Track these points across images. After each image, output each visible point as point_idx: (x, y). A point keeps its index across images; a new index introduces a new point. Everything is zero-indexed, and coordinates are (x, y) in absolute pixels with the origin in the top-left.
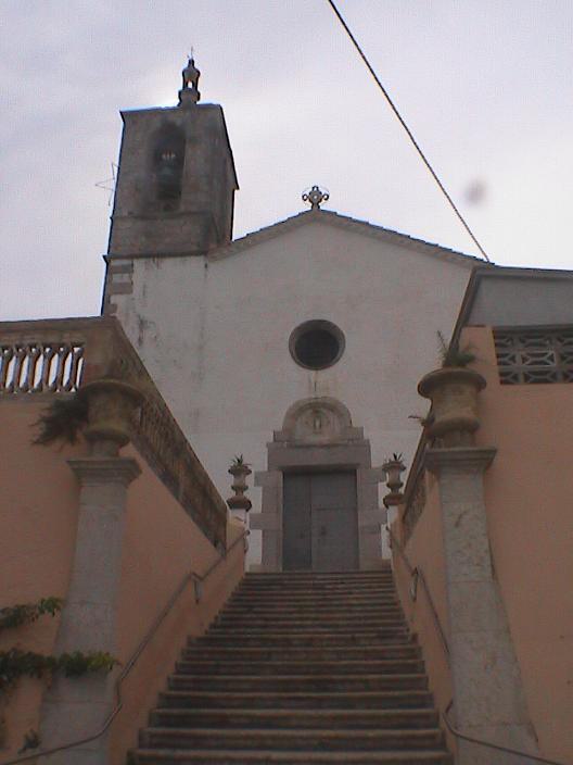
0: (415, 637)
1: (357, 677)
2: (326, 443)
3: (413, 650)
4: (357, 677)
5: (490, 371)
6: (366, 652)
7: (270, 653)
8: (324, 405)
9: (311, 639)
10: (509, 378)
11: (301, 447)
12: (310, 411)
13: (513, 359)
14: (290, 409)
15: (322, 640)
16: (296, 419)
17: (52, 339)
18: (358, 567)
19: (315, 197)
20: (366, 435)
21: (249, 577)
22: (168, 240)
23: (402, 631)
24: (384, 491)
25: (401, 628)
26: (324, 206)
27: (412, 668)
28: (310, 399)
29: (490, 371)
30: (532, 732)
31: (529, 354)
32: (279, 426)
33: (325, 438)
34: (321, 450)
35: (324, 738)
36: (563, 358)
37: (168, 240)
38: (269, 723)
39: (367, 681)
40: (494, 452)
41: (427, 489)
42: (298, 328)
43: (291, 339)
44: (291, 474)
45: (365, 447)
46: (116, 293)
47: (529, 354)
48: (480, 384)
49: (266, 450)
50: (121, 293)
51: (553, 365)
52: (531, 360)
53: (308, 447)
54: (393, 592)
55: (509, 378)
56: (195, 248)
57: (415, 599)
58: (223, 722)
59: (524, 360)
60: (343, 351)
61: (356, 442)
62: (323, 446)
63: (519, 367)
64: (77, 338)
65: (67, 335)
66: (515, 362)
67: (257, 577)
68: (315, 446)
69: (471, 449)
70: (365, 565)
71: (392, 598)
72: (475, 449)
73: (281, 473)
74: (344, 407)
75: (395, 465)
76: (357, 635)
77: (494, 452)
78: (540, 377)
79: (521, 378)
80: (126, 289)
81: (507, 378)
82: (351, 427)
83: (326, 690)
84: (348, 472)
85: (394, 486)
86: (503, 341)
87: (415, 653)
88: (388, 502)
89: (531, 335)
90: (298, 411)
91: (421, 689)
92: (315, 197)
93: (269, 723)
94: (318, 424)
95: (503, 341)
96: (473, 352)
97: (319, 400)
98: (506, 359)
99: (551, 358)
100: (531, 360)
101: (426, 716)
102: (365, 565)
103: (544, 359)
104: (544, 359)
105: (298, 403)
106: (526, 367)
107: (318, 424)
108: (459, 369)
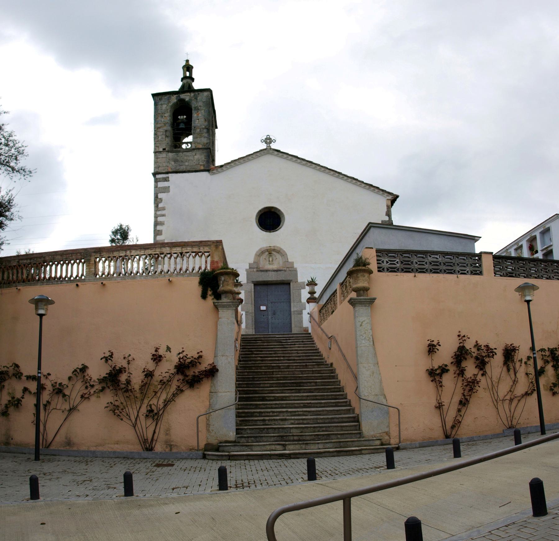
0: (332, 364)
1: (312, 381)
2: (276, 269)
3: (332, 370)
4: (312, 381)
5: (373, 266)
6: (313, 371)
7: (273, 372)
8: (274, 250)
9: (289, 366)
10: (381, 269)
11: (261, 271)
12: (267, 253)
13: (383, 262)
14: (257, 252)
15: (293, 366)
16: (260, 257)
17: (195, 249)
18: (291, 331)
19: (268, 140)
20: (295, 266)
21: (244, 337)
22: (187, 164)
23: (323, 362)
24: (305, 294)
25: (323, 361)
26: (273, 146)
27: (333, 377)
28: (267, 247)
29: (373, 266)
30: (385, 397)
31: (389, 260)
32: (252, 261)
33: (275, 267)
34: (273, 273)
35: (306, 403)
36: (402, 263)
37: (187, 164)
38: (282, 399)
39: (316, 382)
40: (375, 299)
41: (338, 303)
42: (260, 211)
43: (257, 216)
44: (257, 284)
45: (294, 272)
46: (161, 193)
47: (389, 260)
48: (370, 272)
49: (245, 273)
50: (164, 192)
51: (398, 265)
52: (390, 262)
53: (267, 271)
54: (314, 344)
55: (381, 269)
56: (202, 168)
57: (330, 349)
58: (263, 399)
59: (387, 262)
60: (284, 222)
61: (290, 269)
62: (274, 271)
63: (385, 265)
64: (207, 249)
65: (202, 248)
66: (383, 263)
67: (248, 337)
68: (269, 271)
69: (367, 298)
70: (295, 330)
71: (315, 347)
72: (368, 298)
73: (253, 285)
74: (284, 251)
75: (312, 283)
76: (308, 364)
77: (375, 299)
78: (392, 270)
79: (386, 269)
80: (166, 190)
81: (380, 270)
82: (288, 261)
83: (300, 386)
84: (287, 284)
85: (312, 293)
86: (380, 254)
87: (333, 371)
88: (309, 301)
89: (387, 252)
90: (261, 253)
91: (338, 385)
92: (268, 140)
93: (282, 399)
94: (271, 259)
95: (380, 254)
96: (368, 261)
97: (272, 248)
98: (380, 262)
99: (397, 262)
100: (390, 262)
101: (342, 395)
102: (295, 330)
103: (395, 262)
104: (395, 262)
105: (261, 249)
106: (388, 265)
107: (271, 259)
108: (364, 268)
